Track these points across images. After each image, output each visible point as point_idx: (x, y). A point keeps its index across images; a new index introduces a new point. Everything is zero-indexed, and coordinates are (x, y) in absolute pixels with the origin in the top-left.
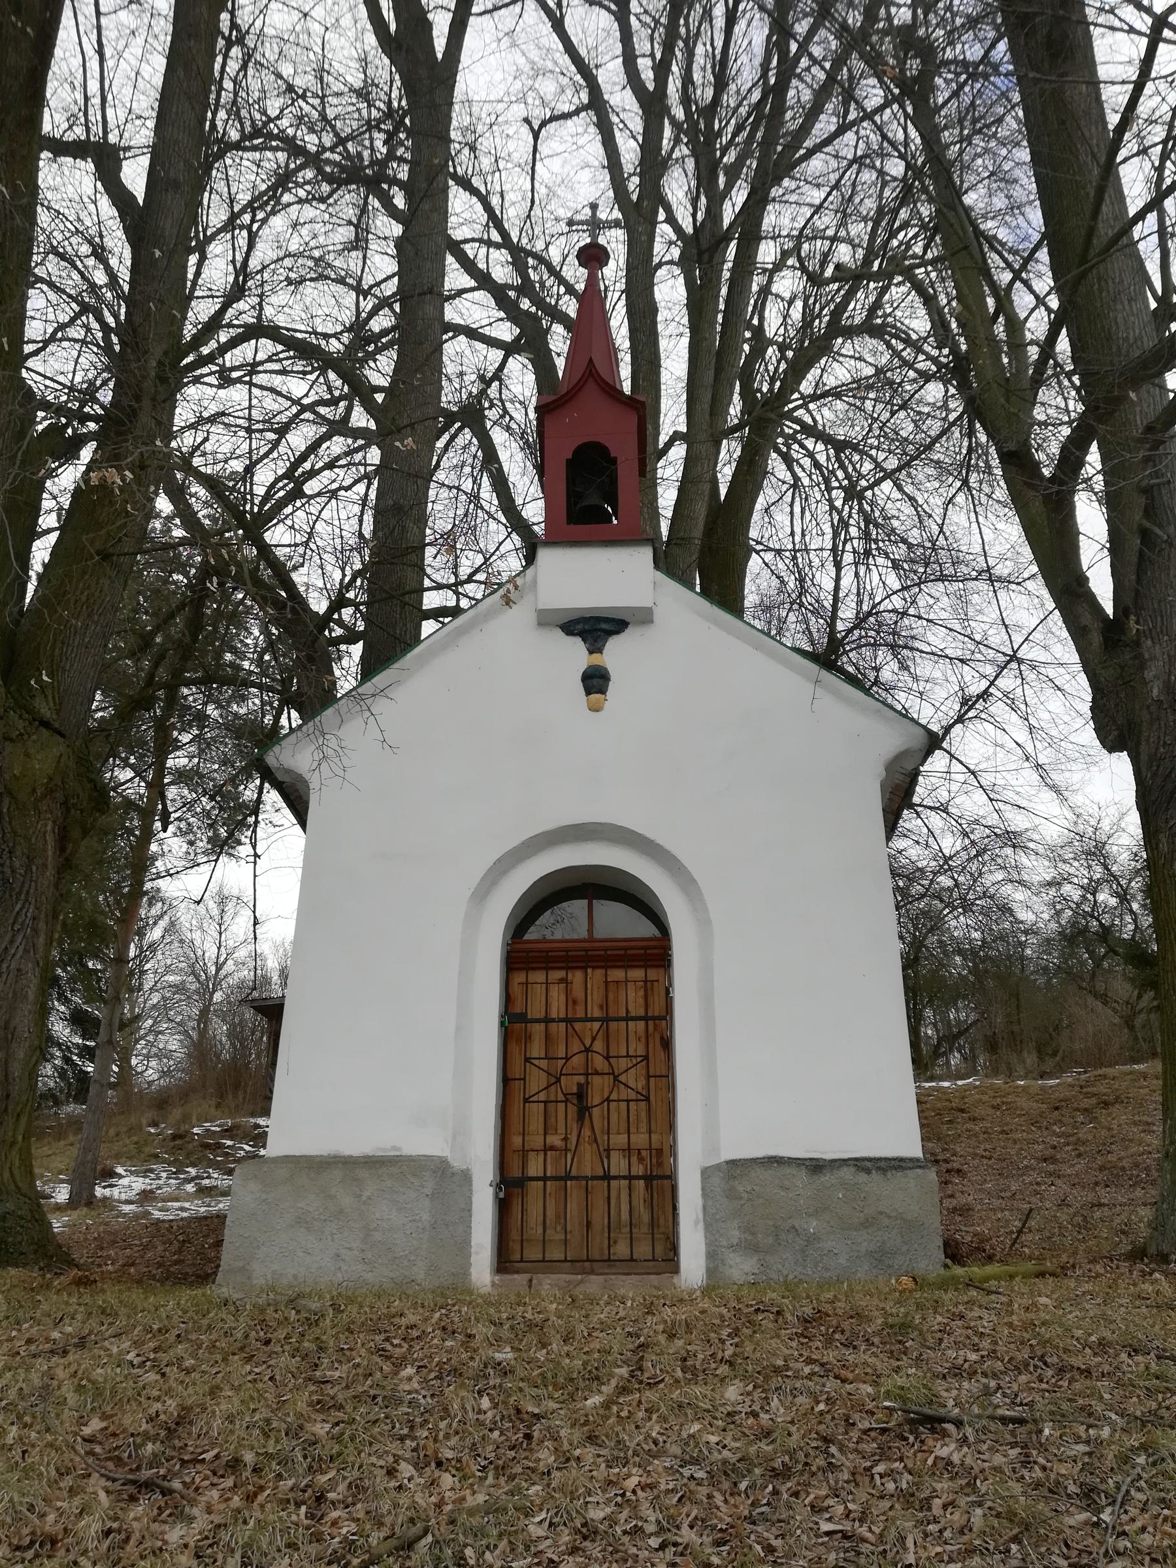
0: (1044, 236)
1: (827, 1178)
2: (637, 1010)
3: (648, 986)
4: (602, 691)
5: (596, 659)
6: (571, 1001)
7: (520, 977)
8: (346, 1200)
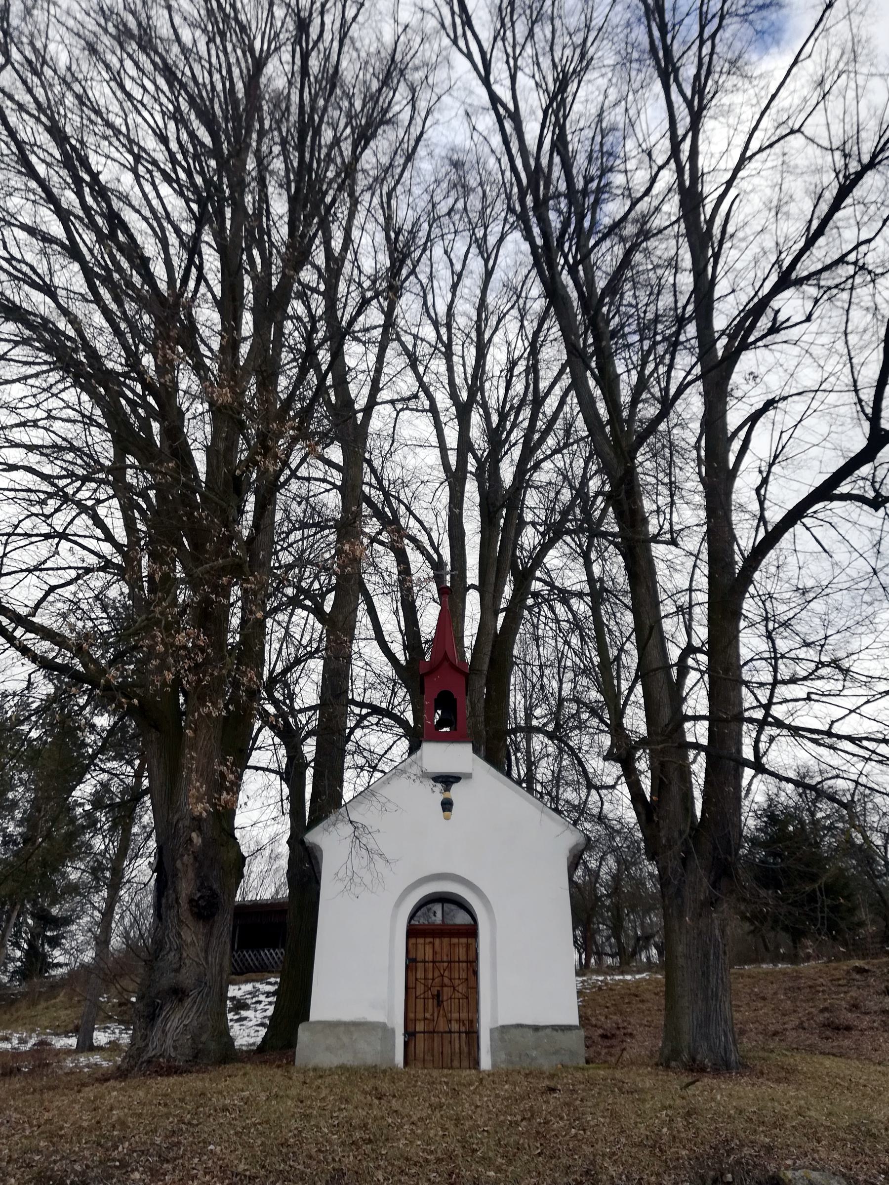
0: (634, 630)
1: (541, 1033)
2: (463, 957)
3: (468, 946)
4: (450, 810)
5: (447, 795)
6: (435, 953)
7: (413, 941)
8: (345, 1040)
